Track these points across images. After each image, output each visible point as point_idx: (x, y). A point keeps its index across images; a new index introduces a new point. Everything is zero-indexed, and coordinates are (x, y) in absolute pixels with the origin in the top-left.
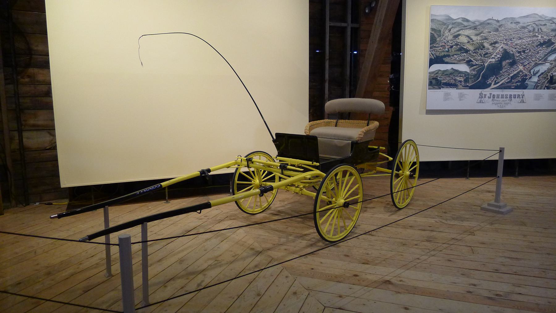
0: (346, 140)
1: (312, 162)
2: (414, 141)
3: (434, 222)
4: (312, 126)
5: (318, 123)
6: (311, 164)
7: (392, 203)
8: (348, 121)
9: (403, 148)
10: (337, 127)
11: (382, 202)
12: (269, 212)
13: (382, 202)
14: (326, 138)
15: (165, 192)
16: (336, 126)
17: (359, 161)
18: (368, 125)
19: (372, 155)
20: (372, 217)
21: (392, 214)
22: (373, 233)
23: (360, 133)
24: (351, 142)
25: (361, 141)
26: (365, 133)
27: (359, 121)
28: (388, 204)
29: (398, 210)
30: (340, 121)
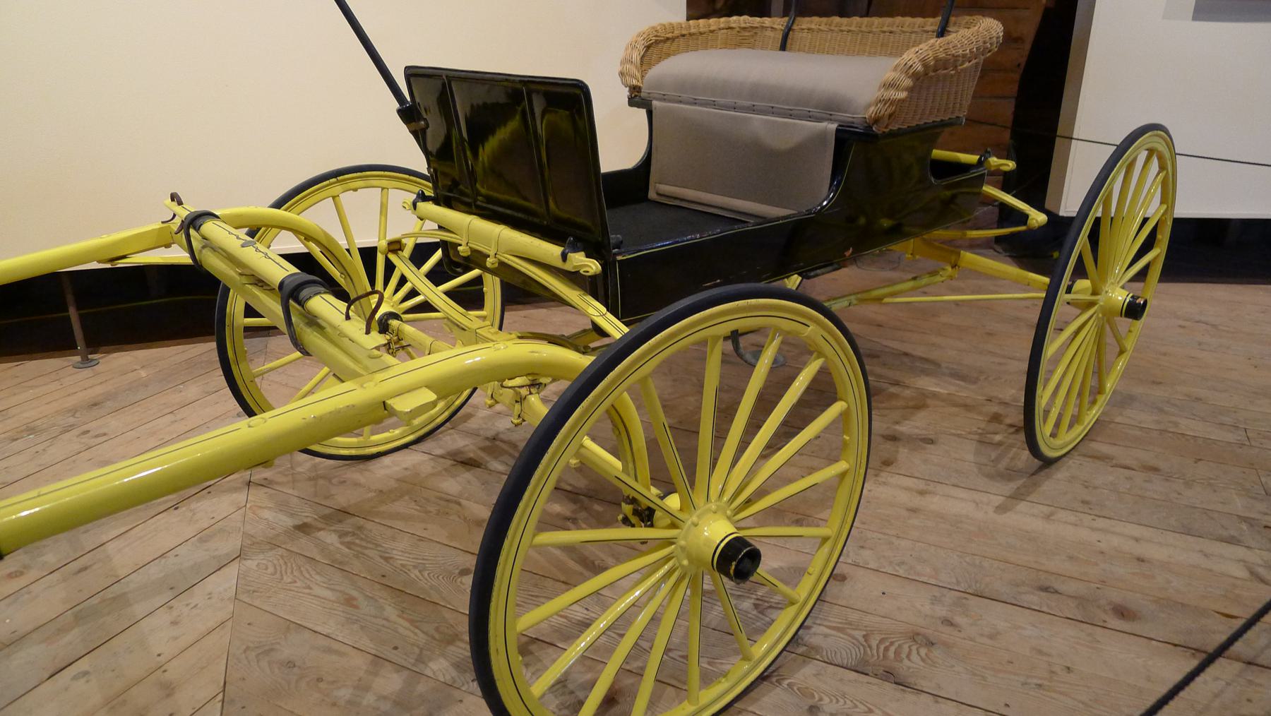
0: (810, 117)
1: (561, 249)
2: (1171, 133)
3: (1240, 572)
4: (657, 42)
5: (693, 31)
6: (558, 263)
7: (1017, 418)
8: (845, 20)
9: (1118, 172)
10: (790, 50)
11: (967, 407)
12: (452, 441)
13: (967, 407)
14: (714, 104)
15: (68, 318)
16: (783, 47)
17: (886, 223)
18: (942, 33)
19: (948, 193)
20: (913, 510)
21: (1017, 496)
22: (906, 662)
23: (890, 75)
24: (834, 126)
25: (894, 127)
26: (916, 76)
27: (899, 19)
28: (996, 418)
29: (1041, 469)
30: (805, 23)
